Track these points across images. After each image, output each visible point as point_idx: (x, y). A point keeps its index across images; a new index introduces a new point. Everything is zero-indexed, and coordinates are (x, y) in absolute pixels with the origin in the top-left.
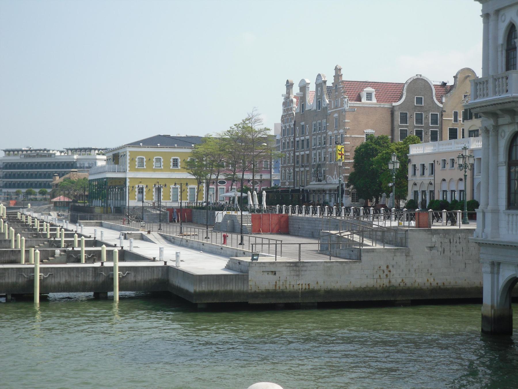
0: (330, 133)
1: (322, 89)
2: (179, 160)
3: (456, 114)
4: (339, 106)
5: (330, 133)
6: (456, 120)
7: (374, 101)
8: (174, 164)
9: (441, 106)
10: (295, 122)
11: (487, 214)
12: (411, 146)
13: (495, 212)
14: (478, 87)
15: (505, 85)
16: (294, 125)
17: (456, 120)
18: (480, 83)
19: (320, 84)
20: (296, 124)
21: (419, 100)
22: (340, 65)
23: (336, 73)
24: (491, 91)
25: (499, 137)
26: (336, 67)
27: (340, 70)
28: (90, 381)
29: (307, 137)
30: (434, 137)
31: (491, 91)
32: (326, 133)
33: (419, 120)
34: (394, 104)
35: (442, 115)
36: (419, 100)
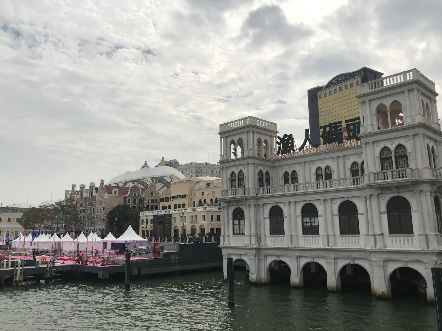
0: (97, 207)
1: (93, 189)
2: (11, 219)
3: (148, 199)
4: (103, 196)
5: (97, 207)
6: (148, 202)
7: (117, 194)
8: (17, 220)
9: (143, 196)
10: (77, 202)
11: (252, 237)
12: (141, 213)
13: (229, 236)
14: (224, 192)
15: (244, 192)
16: (77, 203)
17: (148, 202)
18: (224, 191)
19: (92, 187)
20: (78, 203)
21: (135, 194)
22: (103, 179)
23: (101, 182)
24: (230, 194)
25: (229, 210)
26: (101, 180)
27: (103, 181)
28: (81, 326)
29: (84, 208)
30: (152, 209)
31: (230, 194)
32: (95, 207)
33: (135, 201)
34: (125, 195)
35: (143, 200)
36: (135, 194)
